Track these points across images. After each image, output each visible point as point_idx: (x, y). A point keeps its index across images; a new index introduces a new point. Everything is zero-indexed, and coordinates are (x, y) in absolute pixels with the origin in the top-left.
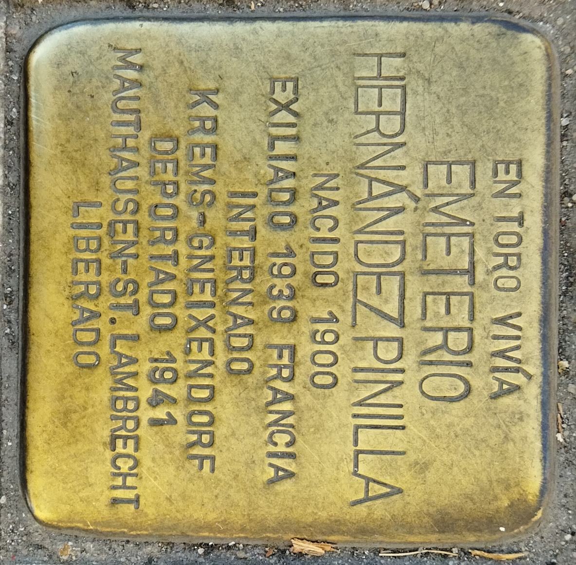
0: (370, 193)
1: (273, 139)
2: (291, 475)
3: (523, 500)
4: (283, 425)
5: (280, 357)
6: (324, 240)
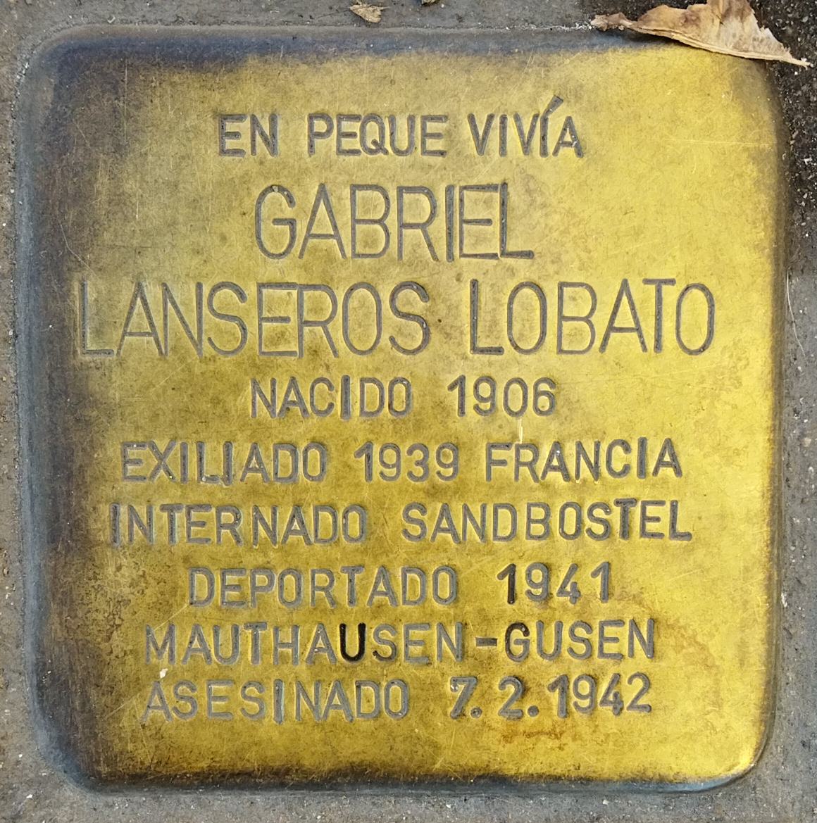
0: (149, 334)
2: (669, 445)
5: (503, 463)
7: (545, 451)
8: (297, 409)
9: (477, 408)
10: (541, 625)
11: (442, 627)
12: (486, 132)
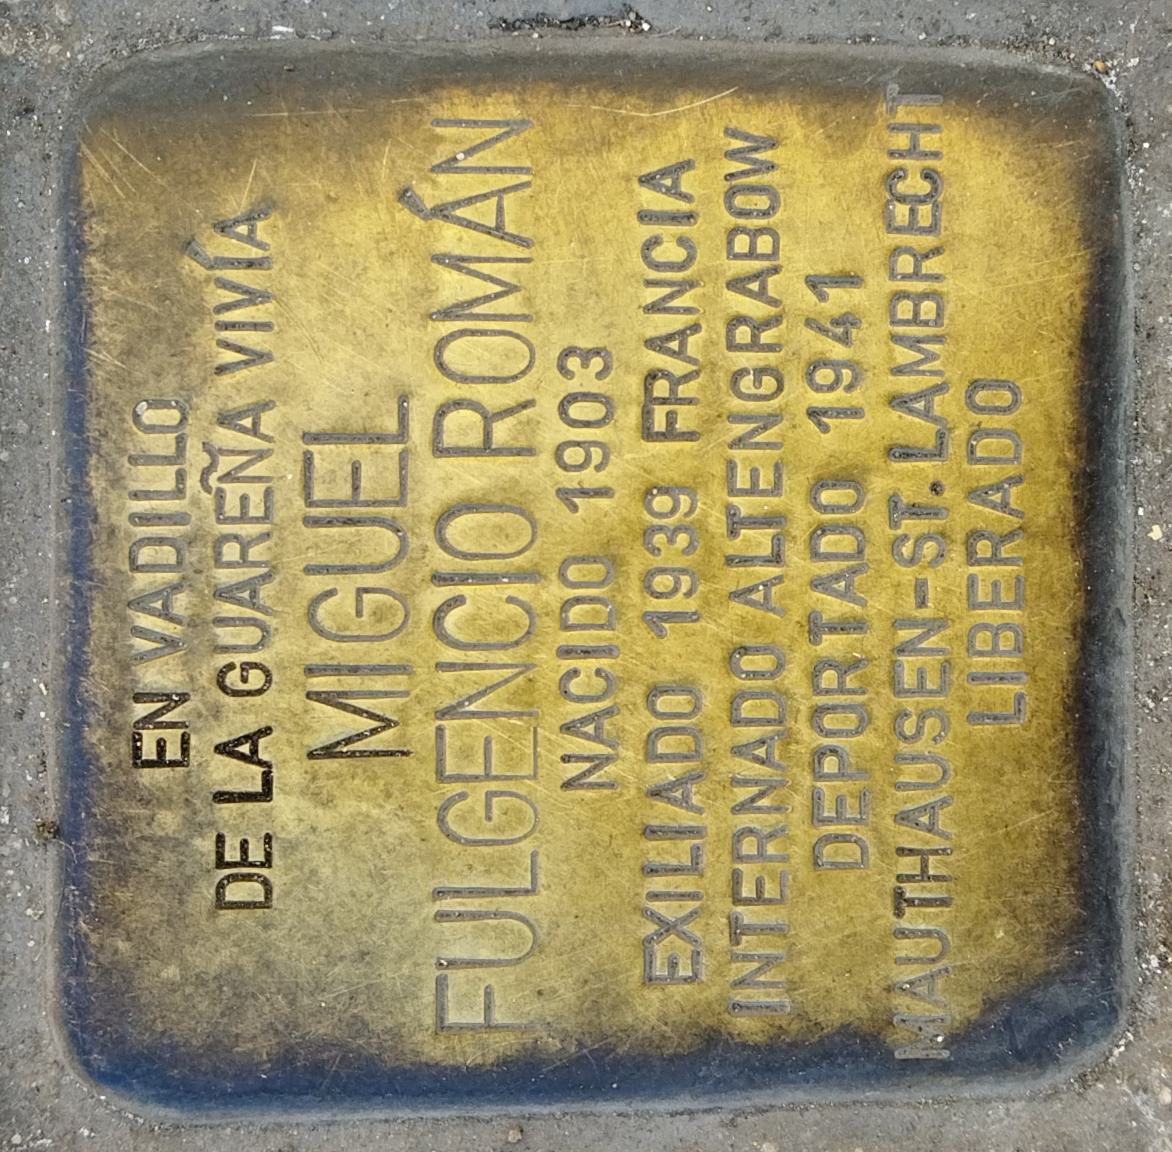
0: (500, 200)
1: (694, 868)
5: (671, 418)
6: (587, 653)
7: (658, 360)
8: (607, 724)
9: (598, 468)
11: (901, 650)
12: (240, 349)
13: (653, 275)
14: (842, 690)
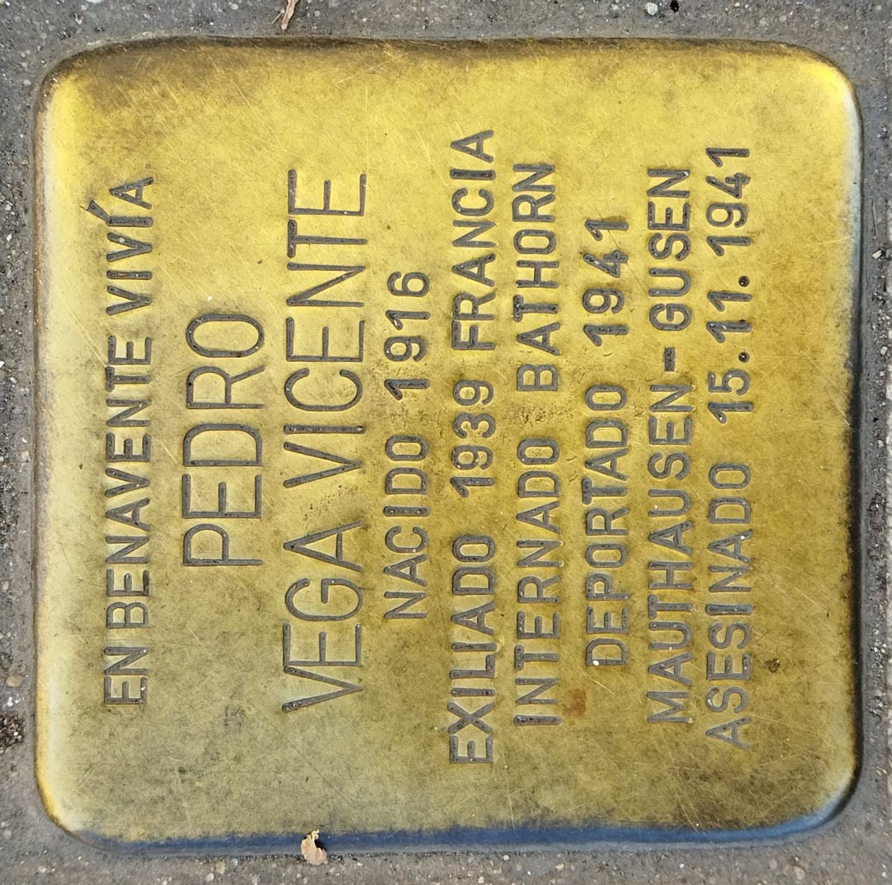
1: (488, 672)
2: (458, 145)
3: (102, 100)
4: (469, 224)
5: (473, 330)
6: (411, 512)
10: (652, 292)
13: (461, 217)
14: (607, 529)
